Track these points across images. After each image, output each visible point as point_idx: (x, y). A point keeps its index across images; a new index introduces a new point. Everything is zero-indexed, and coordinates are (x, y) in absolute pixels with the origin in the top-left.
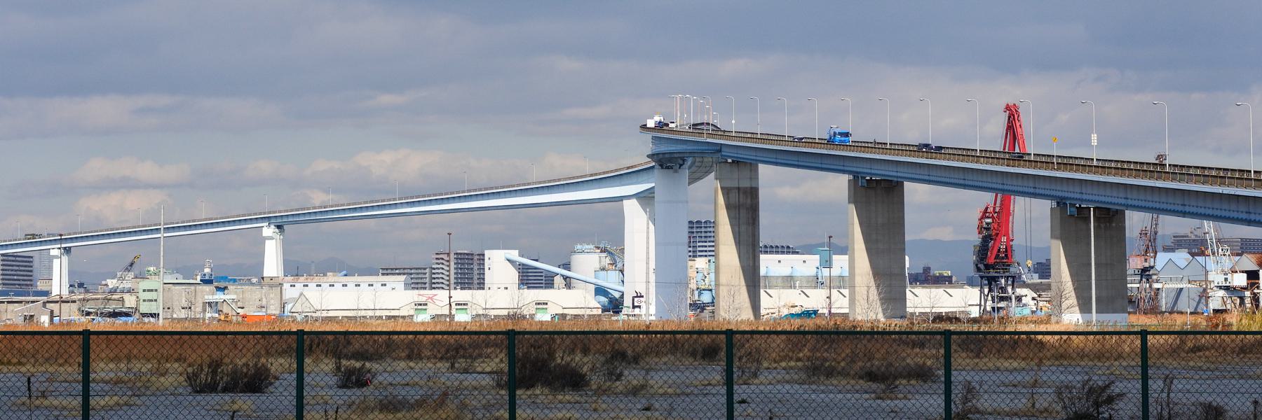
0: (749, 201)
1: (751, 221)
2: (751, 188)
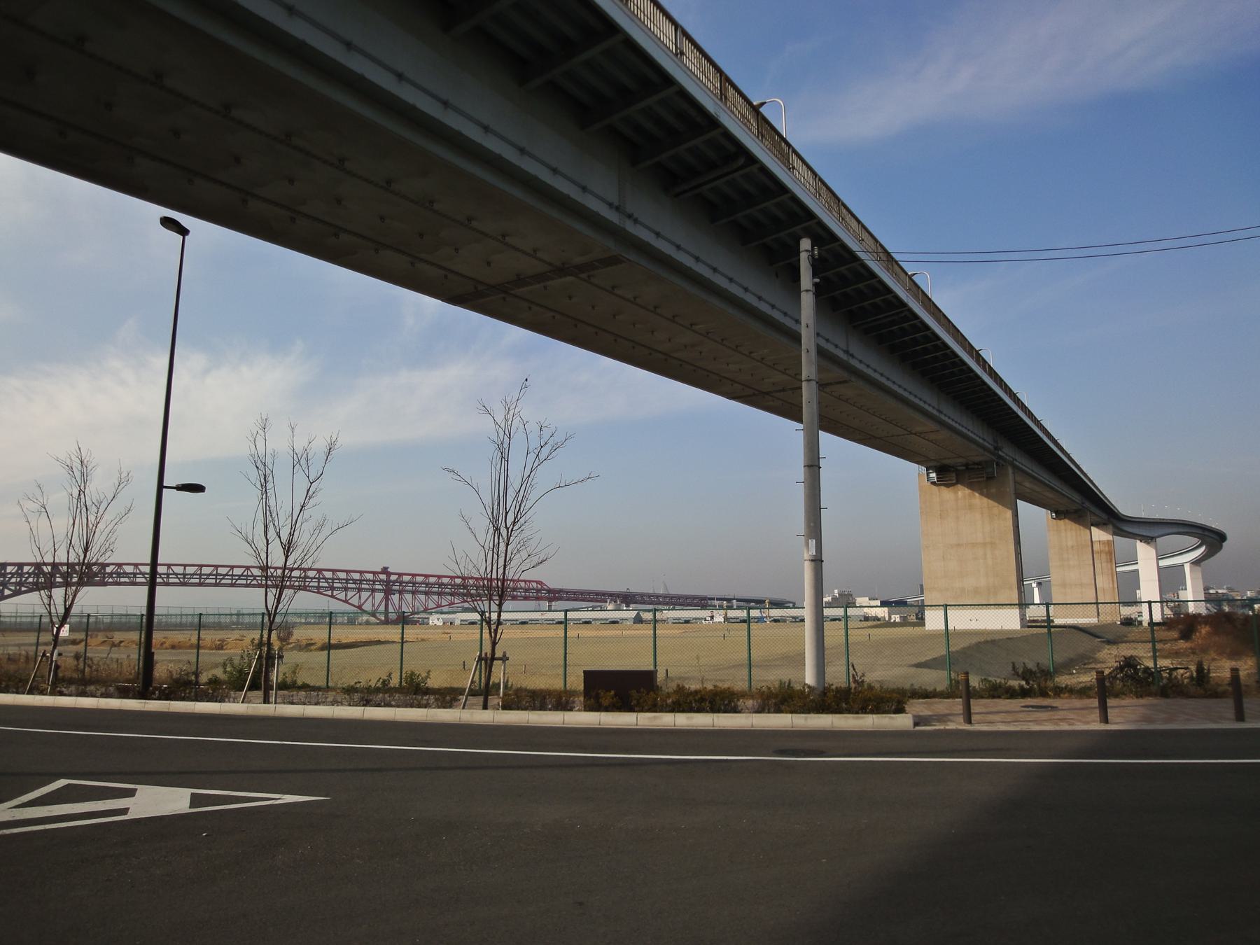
0: (1107, 549)
1: (1109, 560)
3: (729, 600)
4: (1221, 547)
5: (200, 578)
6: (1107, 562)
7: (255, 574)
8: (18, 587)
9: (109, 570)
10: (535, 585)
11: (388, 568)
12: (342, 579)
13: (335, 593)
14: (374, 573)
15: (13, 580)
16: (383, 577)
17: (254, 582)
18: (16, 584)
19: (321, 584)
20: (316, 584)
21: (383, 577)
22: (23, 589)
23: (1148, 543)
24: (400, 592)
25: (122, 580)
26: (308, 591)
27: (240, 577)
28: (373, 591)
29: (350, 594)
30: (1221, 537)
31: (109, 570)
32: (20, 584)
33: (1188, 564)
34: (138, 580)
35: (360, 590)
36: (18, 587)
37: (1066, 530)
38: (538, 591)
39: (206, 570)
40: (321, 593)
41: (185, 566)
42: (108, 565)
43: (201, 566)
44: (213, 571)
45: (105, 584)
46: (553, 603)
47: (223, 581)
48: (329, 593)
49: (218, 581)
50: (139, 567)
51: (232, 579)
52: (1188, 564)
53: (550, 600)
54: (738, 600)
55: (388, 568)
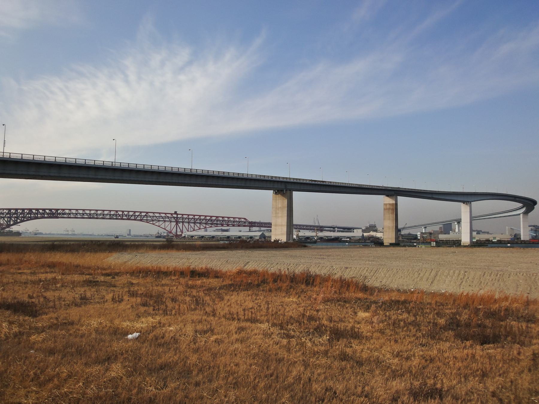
0: (392, 207)
3: (334, 228)
4: (533, 208)
5: (183, 220)
6: (391, 214)
7: (120, 214)
8: (23, 219)
9: (59, 212)
10: (243, 220)
11: (177, 212)
12: (81, 214)
13: (154, 222)
14: (172, 214)
15: (21, 216)
16: (175, 216)
17: (120, 217)
18: (22, 217)
19: (148, 219)
20: (146, 219)
21: (175, 216)
22: (25, 219)
23: (467, 204)
24: (183, 222)
25: (65, 216)
26: (142, 221)
27: (209, 220)
28: (171, 222)
29: (161, 223)
30: (534, 203)
31: (59, 212)
32: (24, 217)
33: (522, 214)
34: (85, 216)
35: (165, 221)
36: (23, 219)
37: (279, 199)
38: (245, 222)
39: (106, 212)
40: (148, 222)
41: (90, 210)
42: (59, 209)
43: (104, 211)
44: (133, 214)
45: (58, 218)
46: (251, 228)
47: (132, 218)
48: (152, 222)
49: (142, 218)
50: (40, 210)
51: (188, 220)
52: (522, 214)
53: (250, 227)
54: (338, 228)
55: (177, 212)
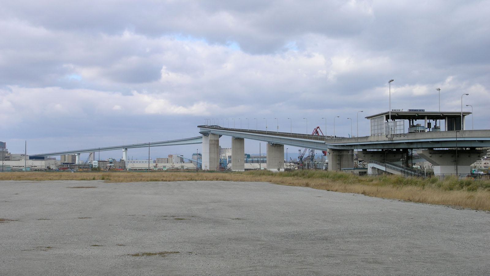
2: (217, 140)
